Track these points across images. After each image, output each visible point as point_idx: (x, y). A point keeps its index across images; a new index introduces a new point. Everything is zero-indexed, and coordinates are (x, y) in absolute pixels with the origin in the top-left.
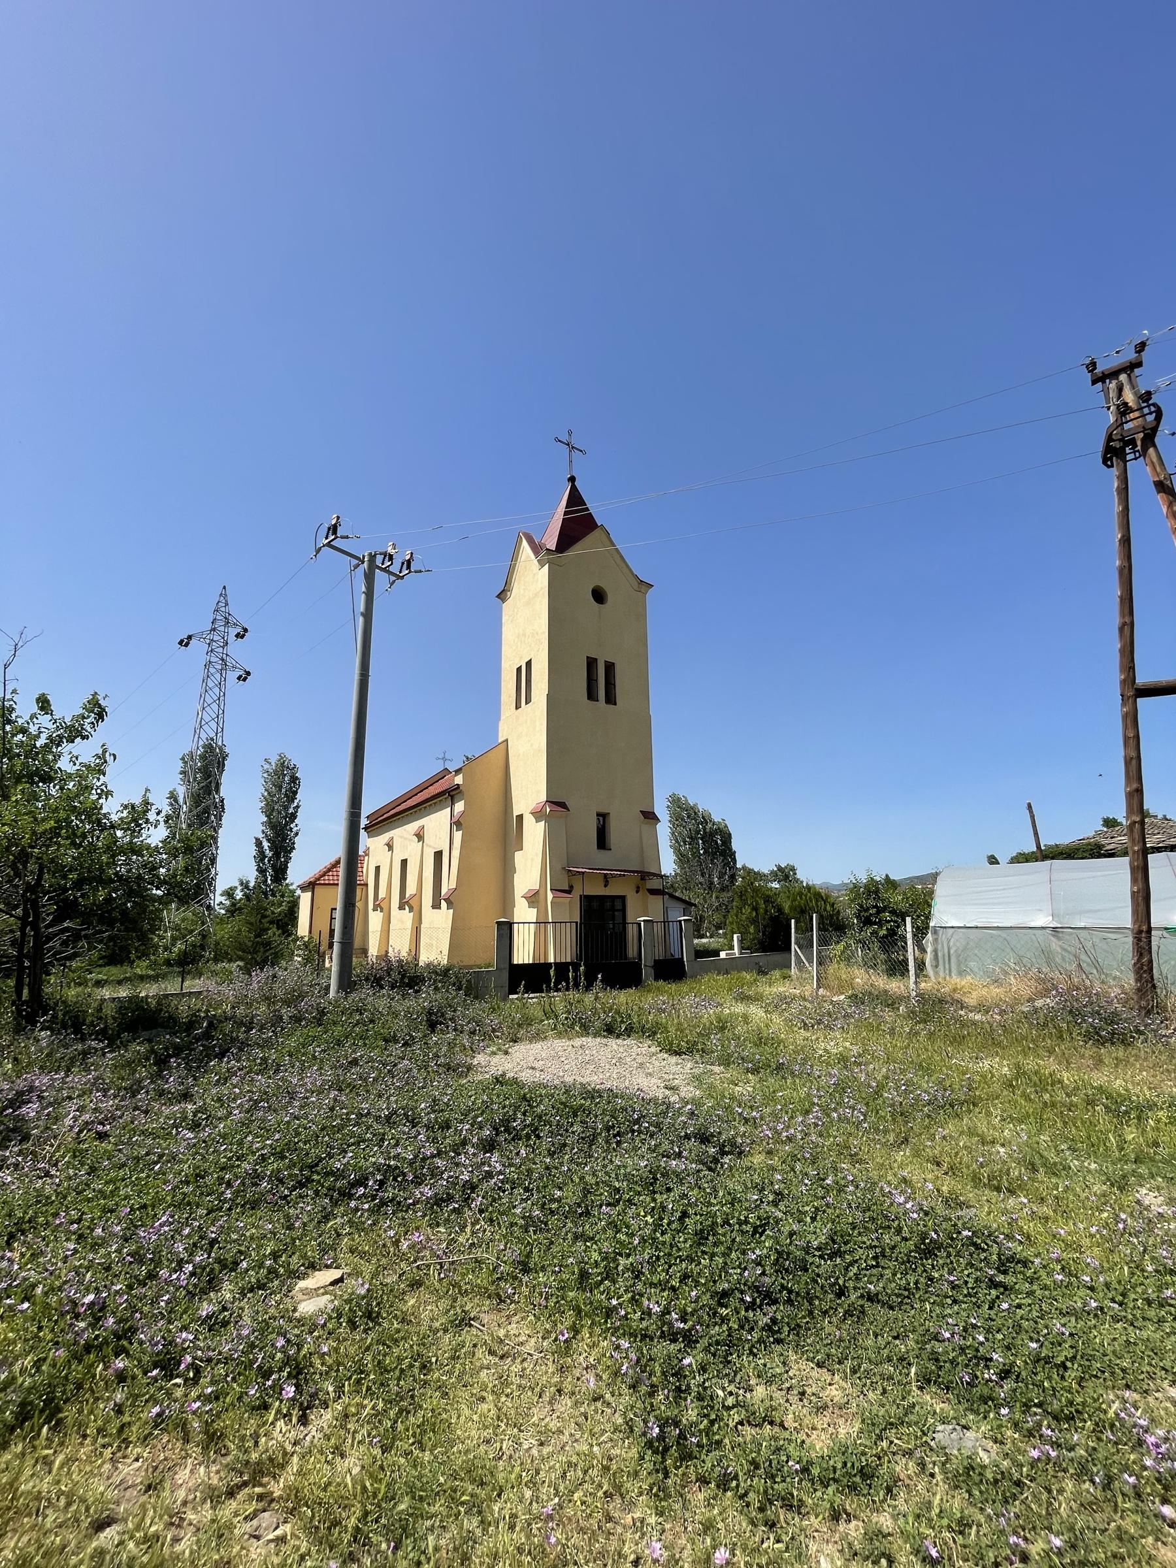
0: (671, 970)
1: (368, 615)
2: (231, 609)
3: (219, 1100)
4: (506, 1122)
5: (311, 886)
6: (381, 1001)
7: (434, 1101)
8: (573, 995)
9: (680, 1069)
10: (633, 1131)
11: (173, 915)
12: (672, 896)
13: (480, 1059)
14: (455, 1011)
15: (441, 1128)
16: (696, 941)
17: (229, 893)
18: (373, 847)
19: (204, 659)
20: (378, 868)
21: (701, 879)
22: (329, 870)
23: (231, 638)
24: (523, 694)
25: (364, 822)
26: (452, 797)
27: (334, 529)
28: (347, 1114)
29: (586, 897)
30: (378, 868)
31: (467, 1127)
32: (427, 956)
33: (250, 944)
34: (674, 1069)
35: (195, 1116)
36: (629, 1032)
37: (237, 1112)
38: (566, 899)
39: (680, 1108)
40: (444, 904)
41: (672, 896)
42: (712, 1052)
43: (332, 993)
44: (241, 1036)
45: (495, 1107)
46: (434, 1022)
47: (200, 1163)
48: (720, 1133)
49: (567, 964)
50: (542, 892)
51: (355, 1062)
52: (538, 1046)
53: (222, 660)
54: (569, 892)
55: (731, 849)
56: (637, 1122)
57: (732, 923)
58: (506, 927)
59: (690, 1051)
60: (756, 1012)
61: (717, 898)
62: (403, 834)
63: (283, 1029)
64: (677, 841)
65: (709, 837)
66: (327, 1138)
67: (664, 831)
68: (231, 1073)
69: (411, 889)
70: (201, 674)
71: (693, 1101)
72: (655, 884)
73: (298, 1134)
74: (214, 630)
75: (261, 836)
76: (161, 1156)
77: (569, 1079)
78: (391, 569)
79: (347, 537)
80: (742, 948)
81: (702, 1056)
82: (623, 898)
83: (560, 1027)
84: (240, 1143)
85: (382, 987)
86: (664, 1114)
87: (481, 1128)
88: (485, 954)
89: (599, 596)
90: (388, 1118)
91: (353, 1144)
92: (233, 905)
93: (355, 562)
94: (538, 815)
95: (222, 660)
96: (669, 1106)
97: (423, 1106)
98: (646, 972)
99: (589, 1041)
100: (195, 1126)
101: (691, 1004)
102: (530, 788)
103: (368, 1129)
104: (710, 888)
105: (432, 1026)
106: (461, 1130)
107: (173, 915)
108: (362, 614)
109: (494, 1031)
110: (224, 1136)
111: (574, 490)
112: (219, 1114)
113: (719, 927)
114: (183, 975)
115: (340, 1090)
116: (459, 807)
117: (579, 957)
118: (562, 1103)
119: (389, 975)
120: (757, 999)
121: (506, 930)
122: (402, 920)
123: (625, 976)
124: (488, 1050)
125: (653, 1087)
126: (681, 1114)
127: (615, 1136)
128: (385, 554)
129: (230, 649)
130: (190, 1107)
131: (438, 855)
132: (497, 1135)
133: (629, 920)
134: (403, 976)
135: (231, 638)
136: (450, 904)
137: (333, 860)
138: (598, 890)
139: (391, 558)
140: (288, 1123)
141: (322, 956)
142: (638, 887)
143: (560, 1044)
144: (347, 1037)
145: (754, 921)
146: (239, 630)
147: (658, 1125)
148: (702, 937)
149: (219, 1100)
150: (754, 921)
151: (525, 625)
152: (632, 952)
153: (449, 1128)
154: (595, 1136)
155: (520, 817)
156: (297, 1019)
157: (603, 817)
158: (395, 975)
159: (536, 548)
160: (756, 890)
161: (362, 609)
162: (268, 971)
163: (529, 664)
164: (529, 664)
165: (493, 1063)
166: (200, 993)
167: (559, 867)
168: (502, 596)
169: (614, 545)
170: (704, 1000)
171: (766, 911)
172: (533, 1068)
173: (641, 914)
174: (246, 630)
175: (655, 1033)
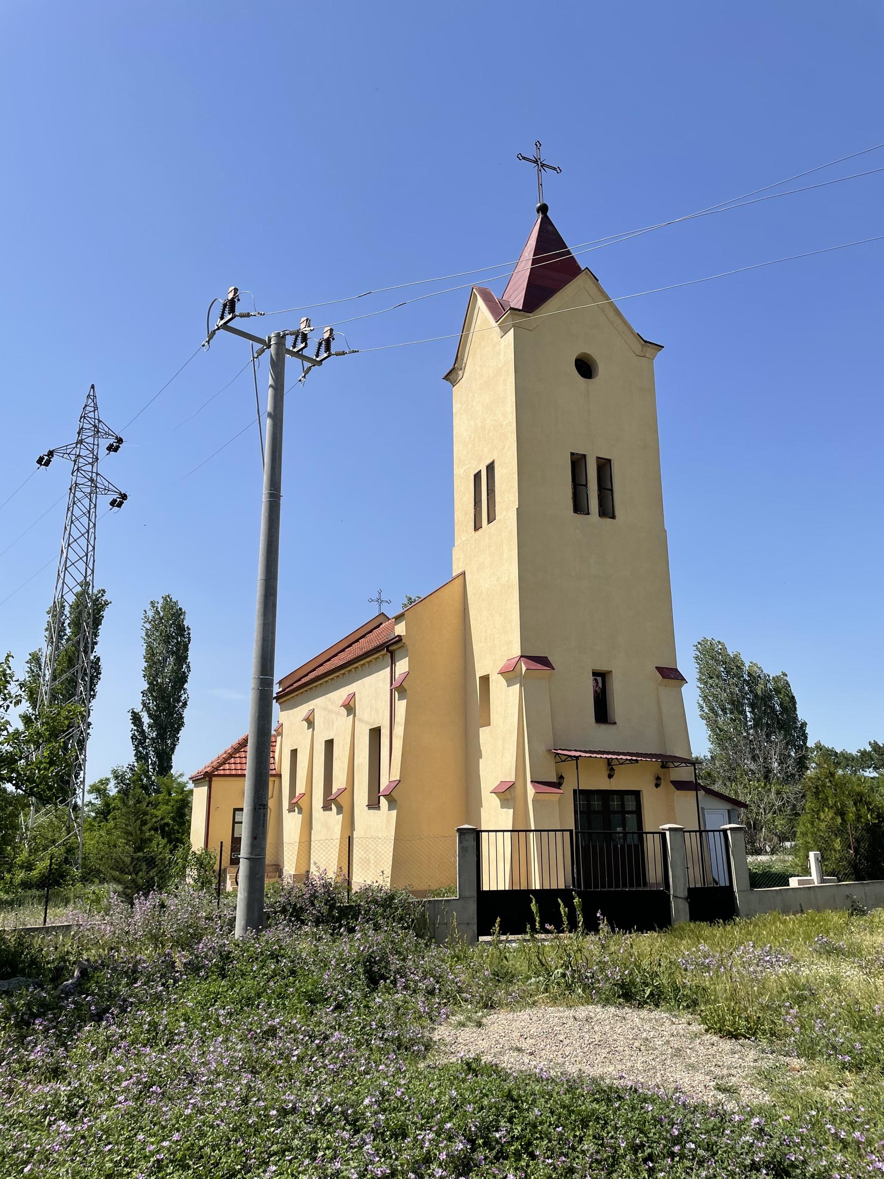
0: (714, 905)
1: (277, 417)
2: (102, 414)
3: (99, 1080)
4: (487, 1129)
5: (207, 778)
6: (303, 943)
7: (382, 1094)
8: (566, 937)
9: (740, 1060)
10: (672, 1155)
11: (33, 819)
12: (710, 792)
13: (442, 1033)
14: (404, 960)
15: (395, 1136)
16: (750, 859)
17: (99, 789)
18: (288, 720)
19: (69, 480)
20: (294, 752)
21: (753, 766)
22: (231, 756)
23: (102, 451)
24: (484, 509)
25: (276, 689)
26: (392, 653)
27: (231, 305)
28: (266, 1108)
29: (583, 792)
30: (294, 752)
31: (432, 1136)
32: (360, 879)
33: (128, 860)
34: (728, 1060)
35: (69, 1101)
36: (656, 999)
37: (121, 1098)
38: (553, 796)
39: (741, 1122)
40: (384, 802)
41: (710, 792)
42: (787, 1035)
43: (238, 932)
44: (124, 991)
45: (470, 1108)
46: (374, 974)
47: (80, 1168)
48: (804, 1162)
49: (557, 893)
50: (519, 786)
51: (271, 1033)
52: (524, 1015)
53: (92, 480)
54: (558, 785)
55: (795, 719)
56: (677, 1140)
57: (804, 834)
58: (471, 838)
59: (752, 1032)
60: (851, 974)
61: (778, 793)
62: (327, 705)
63: (176, 981)
64: (712, 710)
65: (761, 702)
66: (240, 1144)
67: (691, 694)
68: (111, 1044)
69: (339, 782)
70: (66, 500)
71: (760, 1110)
72: (684, 773)
73: (202, 1135)
74: (81, 442)
75: (138, 708)
76: (31, 1154)
77: (572, 1070)
78: (305, 352)
79: (248, 315)
80: (822, 873)
81: (771, 1042)
82: (637, 794)
83: (554, 989)
84: (129, 1142)
85: (303, 922)
86: (718, 1130)
87: (450, 1139)
88: (441, 876)
89: (585, 368)
90: (320, 1117)
91: (275, 1154)
92: (107, 805)
93: (258, 346)
94: (509, 674)
95: (92, 480)
96: (723, 1117)
97: (367, 1102)
98: (678, 908)
99: (596, 1011)
100: (71, 1115)
101: (746, 957)
102: (497, 638)
103: (295, 1132)
104: (766, 777)
105: (373, 981)
106: (423, 1140)
107: (33, 819)
108: (270, 415)
109: (460, 991)
110: (107, 1131)
111: (546, 223)
112: (100, 1100)
113: (783, 838)
114: (46, 901)
115: (254, 1072)
116: (402, 666)
117: (576, 881)
118: (564, 1107)
119: (313, 905)
120: (853, 953)
121: (471, 839)
122: (327, 824)
123: (644, 911)
124: (454, 1019)
125: (695, 1085)
126: (743, 1132)
127: (645, 1161)
128: (296, 334)
129: (101, 467)
130: (63, 1089)
131: (375, 733)
132: (473, 1150)
133: (648, 826)
134: (332, 907)
135: (102, 451)
136: (392, 803)
137: (235, 741)
138: (599, 782)
139: (305, 338)
140: (189, 1117)
141: (221, 876)
142: (658, 778)
143: (555, 1014)
144: (259, 995)
145: (839, 832)
146: (112, 440)
147: (709, 1147)
148: (758, 852)
149: (99, 1080)
150: (839, 832)
151: (485, 410)
152: (654, 874)
153: (405, 1136)
154: (615, 1160)
155: (485, 679)
156: (194, 968)
157: (601, 677)
158: (321, 906)
159: (497, 308)
160: (840, 785)
161: (269, 408)
162: (154, 898)
163: (491, 468)
164: (491, 468)
165: (460, 1039)
166: (68, 927)
167: (541, 749)
168: (452, 376)
169: (607, 298)
170: (768, 953)
171: (859, 817)
172: (519, 1050)
173: (665, 817)
174: (120, 441)
175: (695, 1003)
